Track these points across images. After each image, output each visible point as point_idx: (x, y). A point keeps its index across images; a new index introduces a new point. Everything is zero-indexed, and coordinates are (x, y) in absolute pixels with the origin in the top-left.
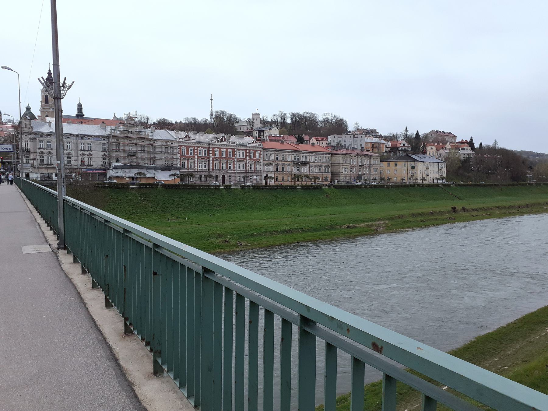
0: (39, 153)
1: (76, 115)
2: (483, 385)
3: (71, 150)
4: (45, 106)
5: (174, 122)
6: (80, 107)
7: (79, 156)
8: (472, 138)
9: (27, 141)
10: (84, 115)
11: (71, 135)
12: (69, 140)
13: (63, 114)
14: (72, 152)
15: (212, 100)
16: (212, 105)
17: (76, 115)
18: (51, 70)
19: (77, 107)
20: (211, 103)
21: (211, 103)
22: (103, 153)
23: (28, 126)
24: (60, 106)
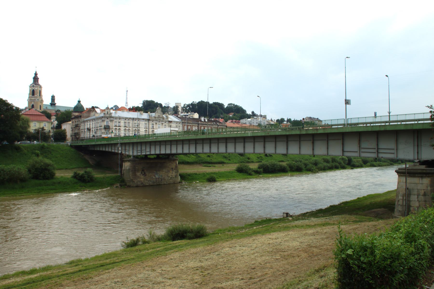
0: (115, 129)
1: (50, 104)
2: (371, 195)
3: (130, 127)
4: (32, 97)
5: (255, 113)
6: (53, 98)
7: (134, 131)
8: (36, 72)
9: (108, 122)
10: (56, 104)
11: (130, 118)
12: (129, 121)
13: (44, 103)
14: (130, 128)
15: (127, 91)
16: (127, 95)
17: (50, 104)
18: (37, 73)
19: (51, 98)
20: (127, 93)
21: (127, 93)
22: (145, 129)
23: (109, 113)
24: (359, 119)
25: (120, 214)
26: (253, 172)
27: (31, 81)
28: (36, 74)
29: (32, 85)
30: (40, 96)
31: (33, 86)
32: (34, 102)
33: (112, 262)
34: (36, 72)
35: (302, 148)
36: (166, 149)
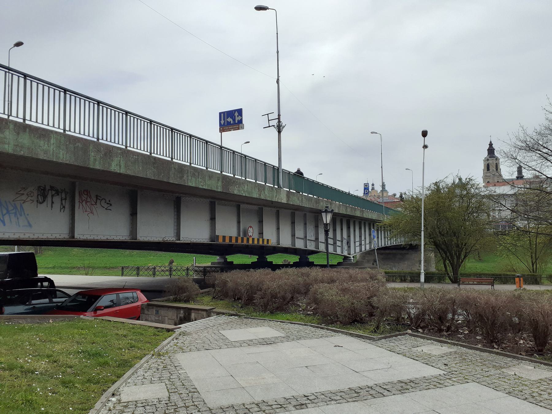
1: (517, 177)
4: (487, 173)
8: (491, 142)
25: (278, 271)
26: (421, 281)
27: (486, 154)
28: (491, 145)
29: (486, 159)
30: (497, 170)
31: (488, 160)
32: (489, 178)
33: (509, 359)
34: (491, 142)
35: (140, 217)
36: (48, 202)
